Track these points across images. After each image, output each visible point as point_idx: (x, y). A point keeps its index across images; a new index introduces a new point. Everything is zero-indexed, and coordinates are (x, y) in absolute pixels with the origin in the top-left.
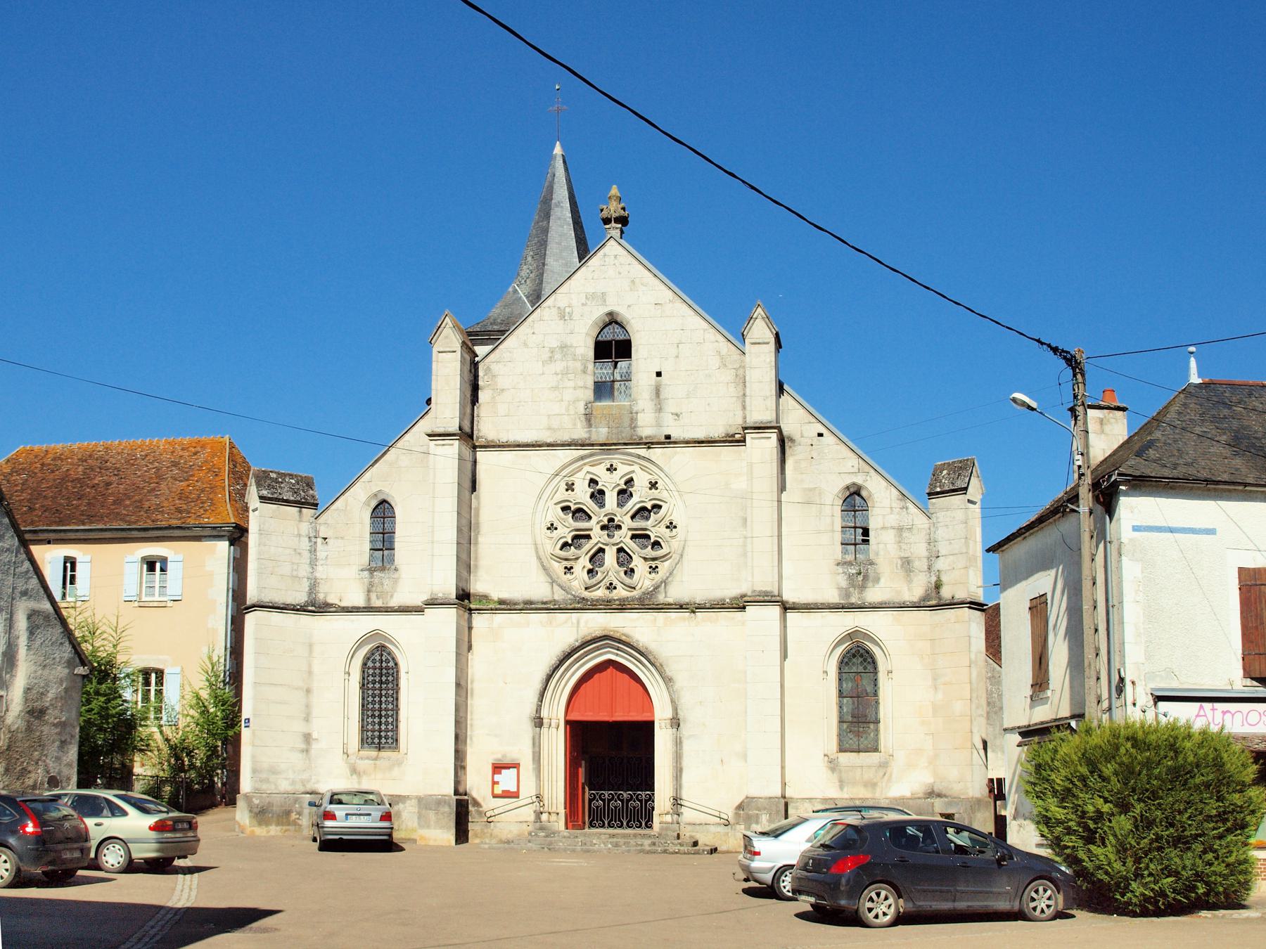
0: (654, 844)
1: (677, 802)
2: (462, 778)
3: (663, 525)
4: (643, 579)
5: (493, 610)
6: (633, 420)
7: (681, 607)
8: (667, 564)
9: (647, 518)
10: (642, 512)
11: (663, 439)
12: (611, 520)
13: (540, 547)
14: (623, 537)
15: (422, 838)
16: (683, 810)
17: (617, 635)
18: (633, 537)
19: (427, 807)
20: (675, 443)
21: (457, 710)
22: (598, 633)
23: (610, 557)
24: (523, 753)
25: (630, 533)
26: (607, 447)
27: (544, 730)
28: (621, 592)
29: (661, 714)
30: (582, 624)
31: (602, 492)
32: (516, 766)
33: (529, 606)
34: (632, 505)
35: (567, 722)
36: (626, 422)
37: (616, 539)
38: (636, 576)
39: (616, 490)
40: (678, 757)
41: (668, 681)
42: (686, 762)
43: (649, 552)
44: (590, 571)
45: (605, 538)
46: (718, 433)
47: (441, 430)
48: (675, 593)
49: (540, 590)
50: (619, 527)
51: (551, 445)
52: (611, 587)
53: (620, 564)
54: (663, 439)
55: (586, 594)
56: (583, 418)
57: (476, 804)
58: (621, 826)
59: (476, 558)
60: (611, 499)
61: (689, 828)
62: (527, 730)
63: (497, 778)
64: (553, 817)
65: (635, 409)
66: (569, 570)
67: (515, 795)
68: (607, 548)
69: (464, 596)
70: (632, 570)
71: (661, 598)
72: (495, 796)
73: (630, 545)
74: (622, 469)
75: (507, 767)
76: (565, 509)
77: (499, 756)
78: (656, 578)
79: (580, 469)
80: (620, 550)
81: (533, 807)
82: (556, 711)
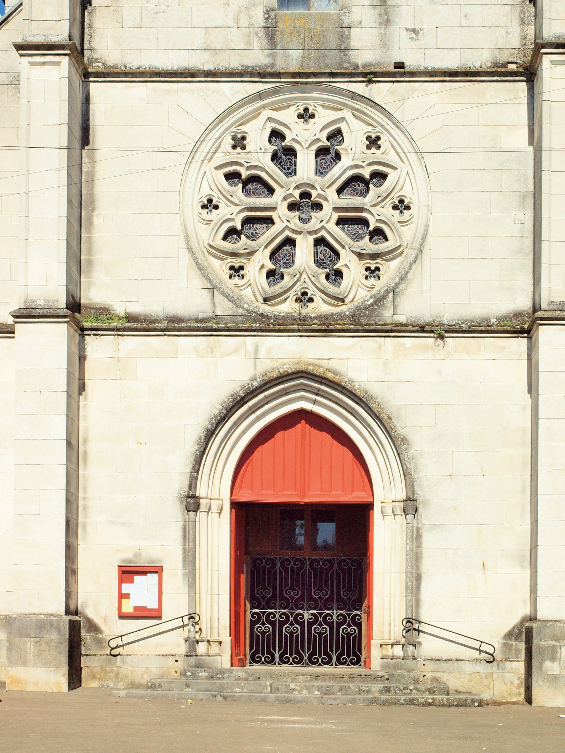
0: (387, 690)
1: (412, 625)
2: (73, 589)
3: (388, 204)
4: (356, 286)
5: (119, 331)
6: (343, 38)
7: (422, 329)
8: (394, 264)
9: (364, 193)
10: (356, 183)
11: (391, 69)
12: (305, 195)
13: (192, 234)
14: (325, 220)
15: (14, 680)
16: (422, 638)
17: (320, 371)
18: (341, 222)
19: (23, 633)
20: (412, 74)
21: (68, 483)
22: (288, 368)
23: (304, 251)
24: (165, 548)
25: (336, 216)
26: (301, 78)
27: (201, 516)
28: (320, 307)
29: (386, 491)
30: (262, 353)
31: (290, 152)
32: (157, 570)
33: (174, 325)
34: (340, 171)
35: (234, 505)
36: (333, 39)
37: (314, 224)
38: (346, 282)
39: (314, 148)
40: (415, 558)
41: (398, 442)
42: (427, 567)
43: (367, 245)
44: (271, 274)
45: (296, 224)
46: (480, 60)
47: (39, 40)
48: (410, 307)
49: (193, 301)
50: (318, 206)
51: (212, 75)
52: (305, 298)
53: (319, 263)
54: (391, 69)
55: (266, 309)
56: (262, 33)
57: (93, 627)
58: (329, 662)
59: (90, 250)
60: (305, 163)
61: (430, 666)
62: (175, 513)
63: (126, 588)
64: (214, 649)
65: (346, 21)
66: (236, 271)
67: (155, 615)
68: (299, 239)
69: (74, 306)
70: (339, 274)
71: (387, 315)
72: (122, 616)
73: (338, 235)
74: (324, 116)
75: (143, 572)
76: (231, 177)
77: (129, 555)
78: (379, 285)
79: (256, 114)
80: (320, 242)
81: (184, 633)
82: (217, 488)
